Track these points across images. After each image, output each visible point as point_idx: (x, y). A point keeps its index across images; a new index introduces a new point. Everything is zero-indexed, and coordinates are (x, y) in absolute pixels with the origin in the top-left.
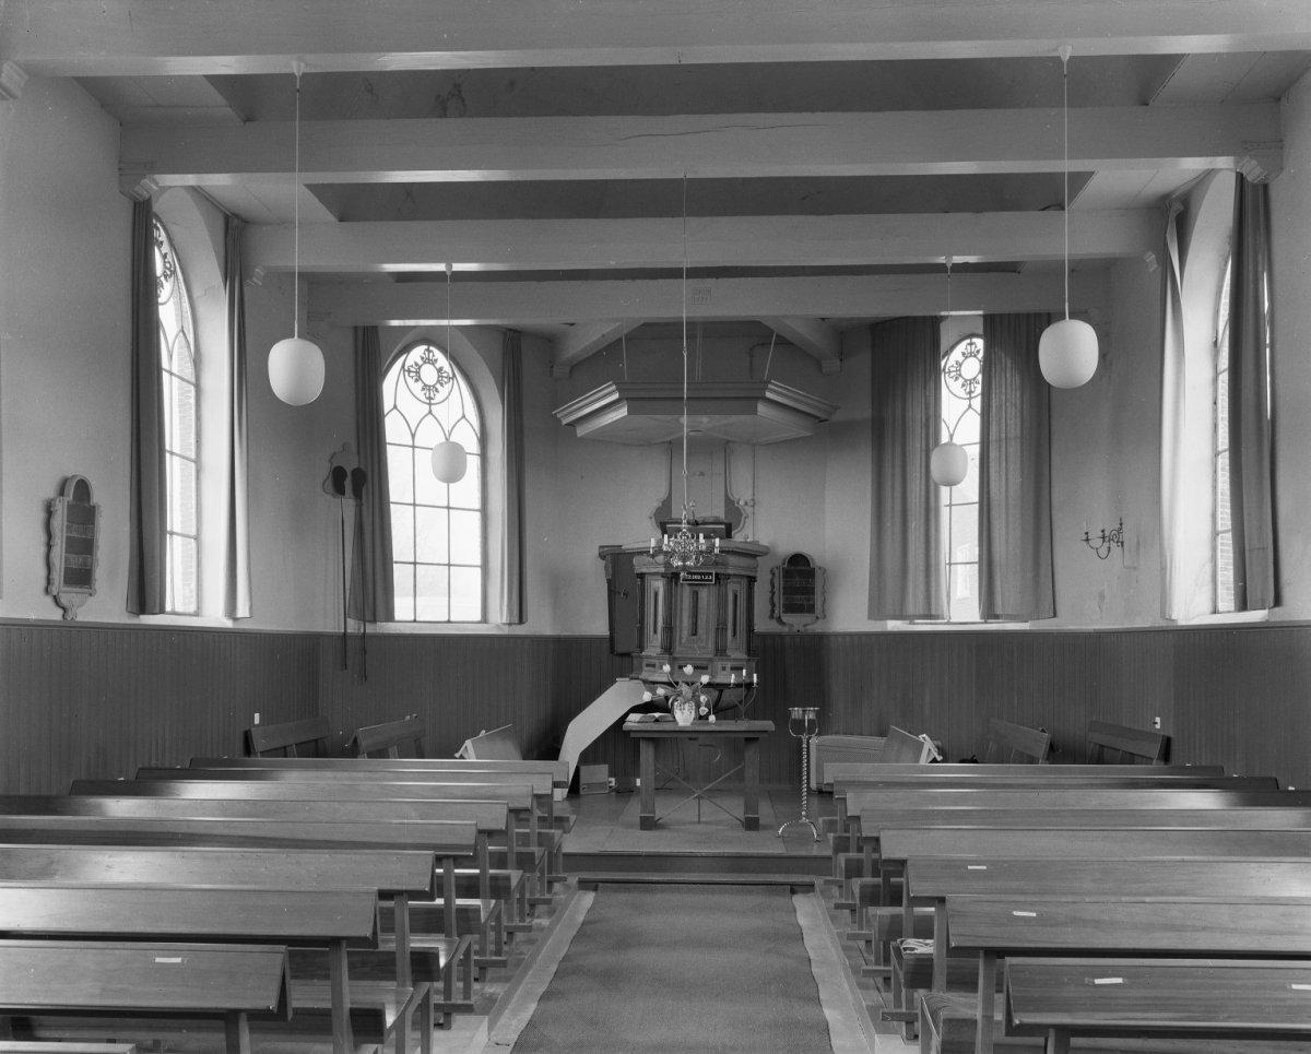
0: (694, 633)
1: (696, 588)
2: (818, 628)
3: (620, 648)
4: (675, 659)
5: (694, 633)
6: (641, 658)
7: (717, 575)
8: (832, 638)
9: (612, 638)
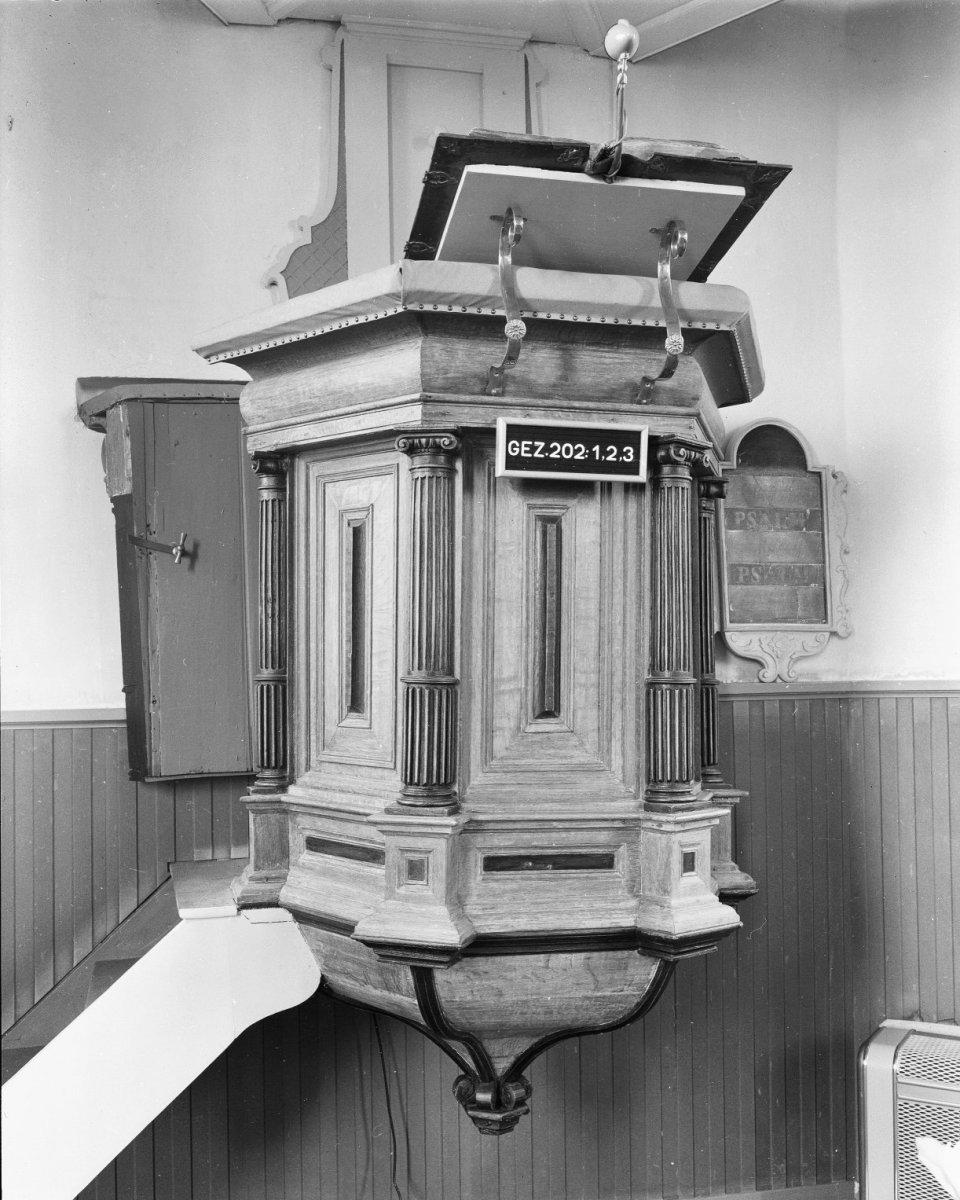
0: (548, 707)
1: (550, 504)
2: (825, 665)
3: (166, 759)
4: (473, 827)
5: (356, 703)
6: (284, 810)
7: (655, 442)
8: (887, 705)
9: (136, 724)
